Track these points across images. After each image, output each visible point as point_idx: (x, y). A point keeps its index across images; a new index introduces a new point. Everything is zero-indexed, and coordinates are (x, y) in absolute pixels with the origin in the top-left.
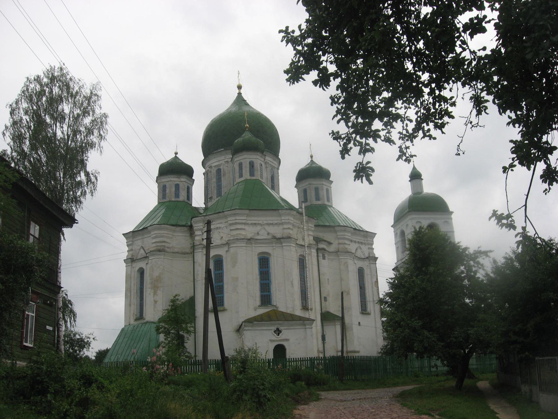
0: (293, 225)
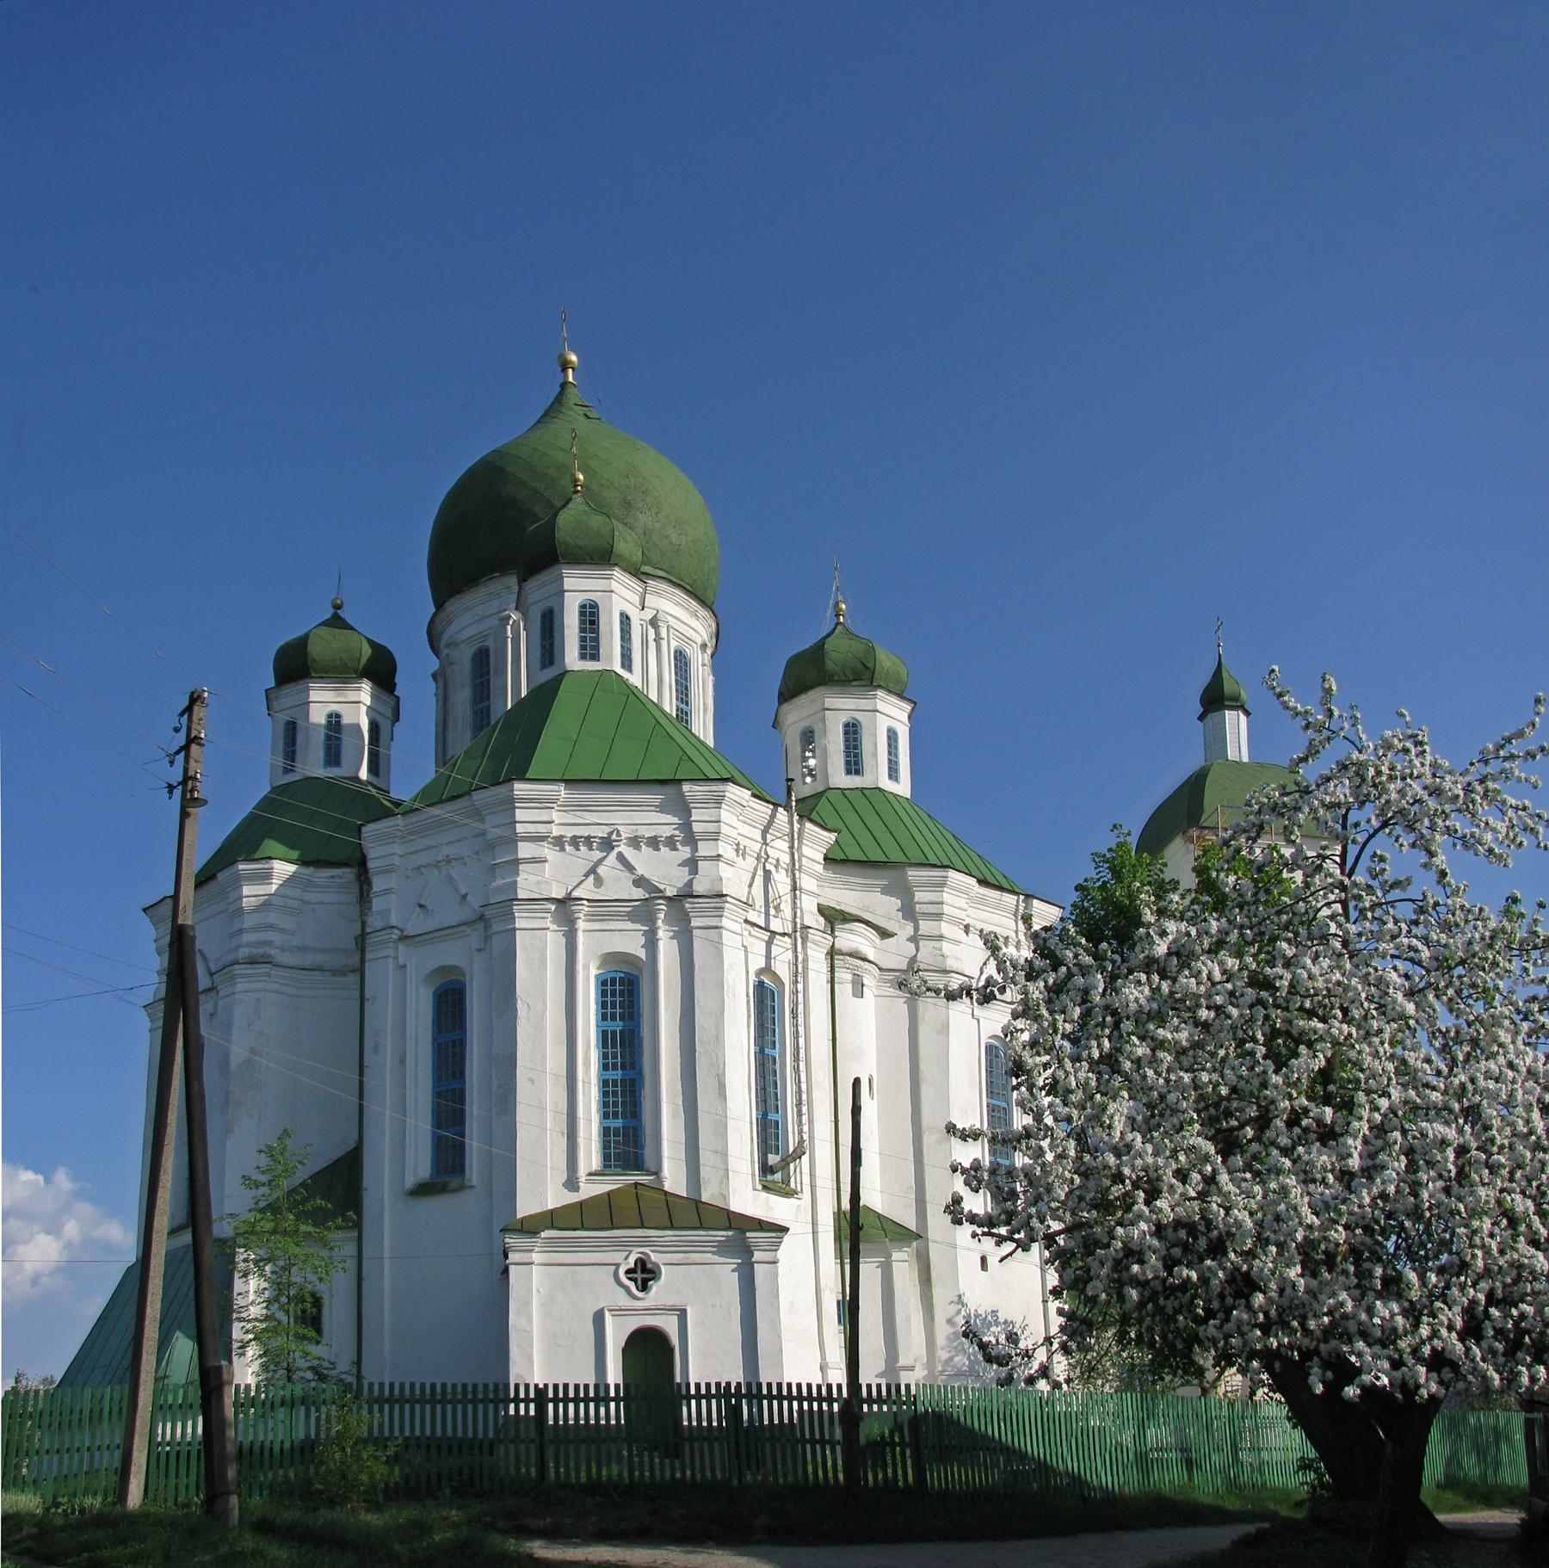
0: (738, 845)
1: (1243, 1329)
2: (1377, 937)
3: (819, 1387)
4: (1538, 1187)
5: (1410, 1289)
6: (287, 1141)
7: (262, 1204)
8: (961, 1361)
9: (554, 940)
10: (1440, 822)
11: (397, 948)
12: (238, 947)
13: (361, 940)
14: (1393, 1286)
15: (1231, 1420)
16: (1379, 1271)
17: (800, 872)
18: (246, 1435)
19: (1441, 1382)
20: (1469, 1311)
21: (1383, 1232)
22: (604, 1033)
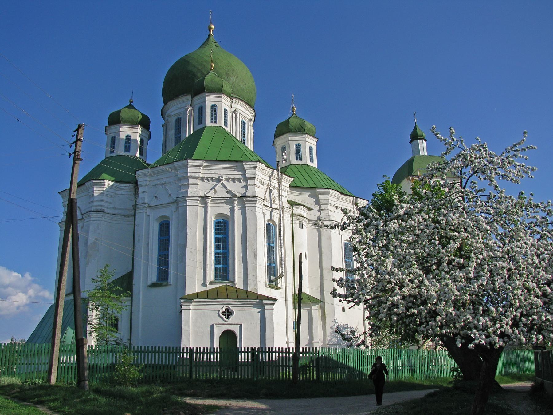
0: (261, 181)
1: (433, 327)
2: (475, 206)
3: (286, 349)
4: (537, 280)
5: (493, 313)
6: (107, 268)
7: (98, 288)
8: (335, 340)
9: (200, 209)
10: (493, 171)
11: (147, 210)
12: (92, 206)
13: (135, 207)
14: (486, 312)
15: (428, 356)
16: (481, 308)
17: (281, 190)
18: (91, 361)
19: (504, 342)
20: (514, 319)
21: (482, 296)
22: (216, 239)
